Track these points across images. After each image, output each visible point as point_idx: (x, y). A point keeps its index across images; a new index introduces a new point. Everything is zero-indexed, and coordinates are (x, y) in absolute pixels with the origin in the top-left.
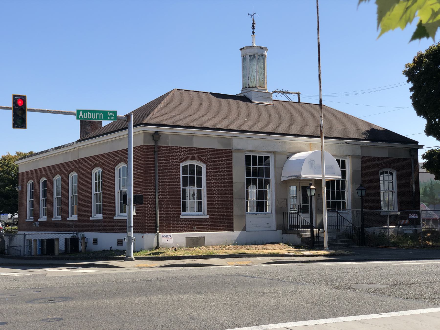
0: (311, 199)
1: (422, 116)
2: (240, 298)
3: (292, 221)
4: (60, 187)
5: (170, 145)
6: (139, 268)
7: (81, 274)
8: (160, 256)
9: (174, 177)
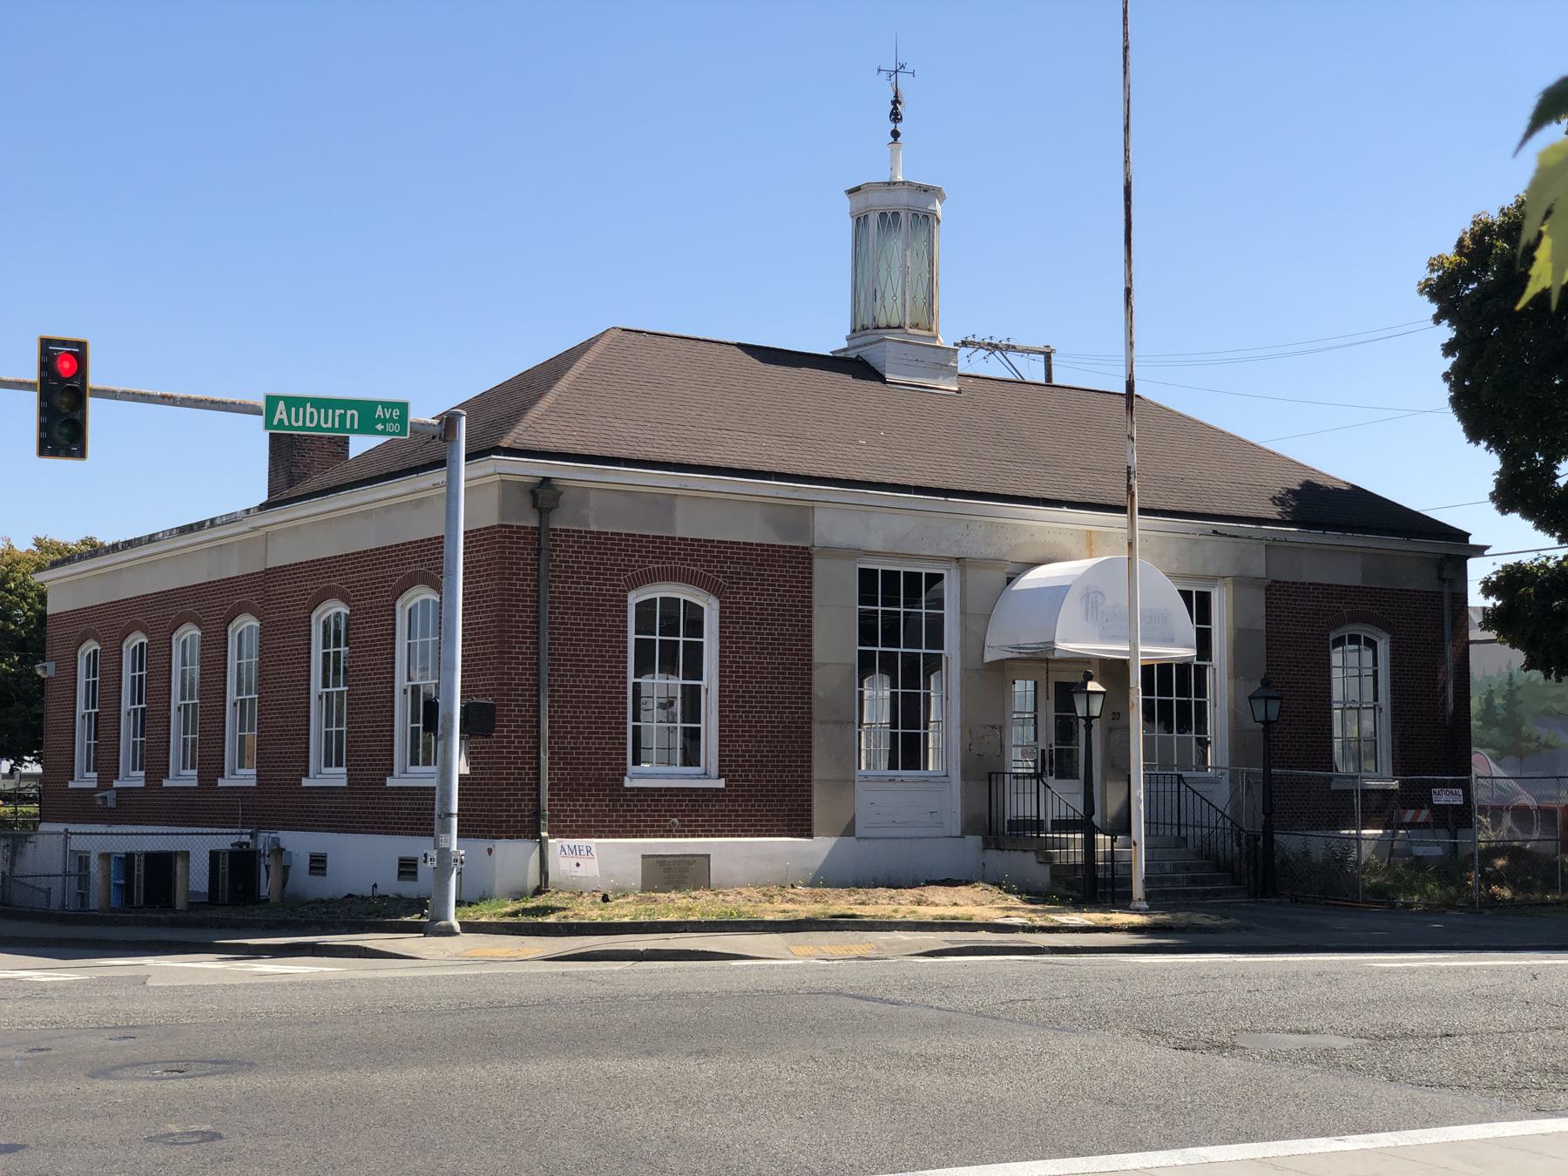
0: (1089, 727)
1: (1484, 444)
2: (843, 1072)
3: (1020, 804)
4: (197, 667)
5: (594, 528)
6: (475, 961)
7: (270, 980)
8: (552, 919)
9: (613, 638)
